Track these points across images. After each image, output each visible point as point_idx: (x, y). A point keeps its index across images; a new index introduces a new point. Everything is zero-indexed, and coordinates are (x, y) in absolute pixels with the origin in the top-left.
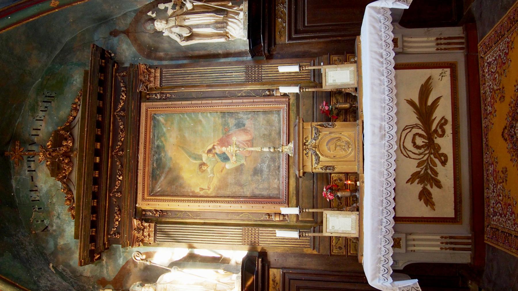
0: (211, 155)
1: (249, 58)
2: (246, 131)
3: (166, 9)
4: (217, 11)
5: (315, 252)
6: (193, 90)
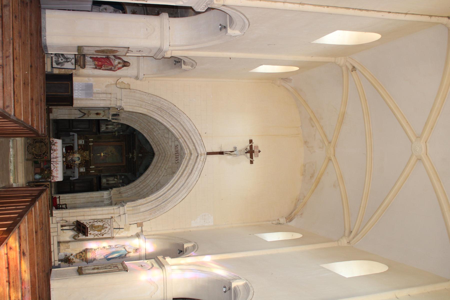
1: (102, 175)
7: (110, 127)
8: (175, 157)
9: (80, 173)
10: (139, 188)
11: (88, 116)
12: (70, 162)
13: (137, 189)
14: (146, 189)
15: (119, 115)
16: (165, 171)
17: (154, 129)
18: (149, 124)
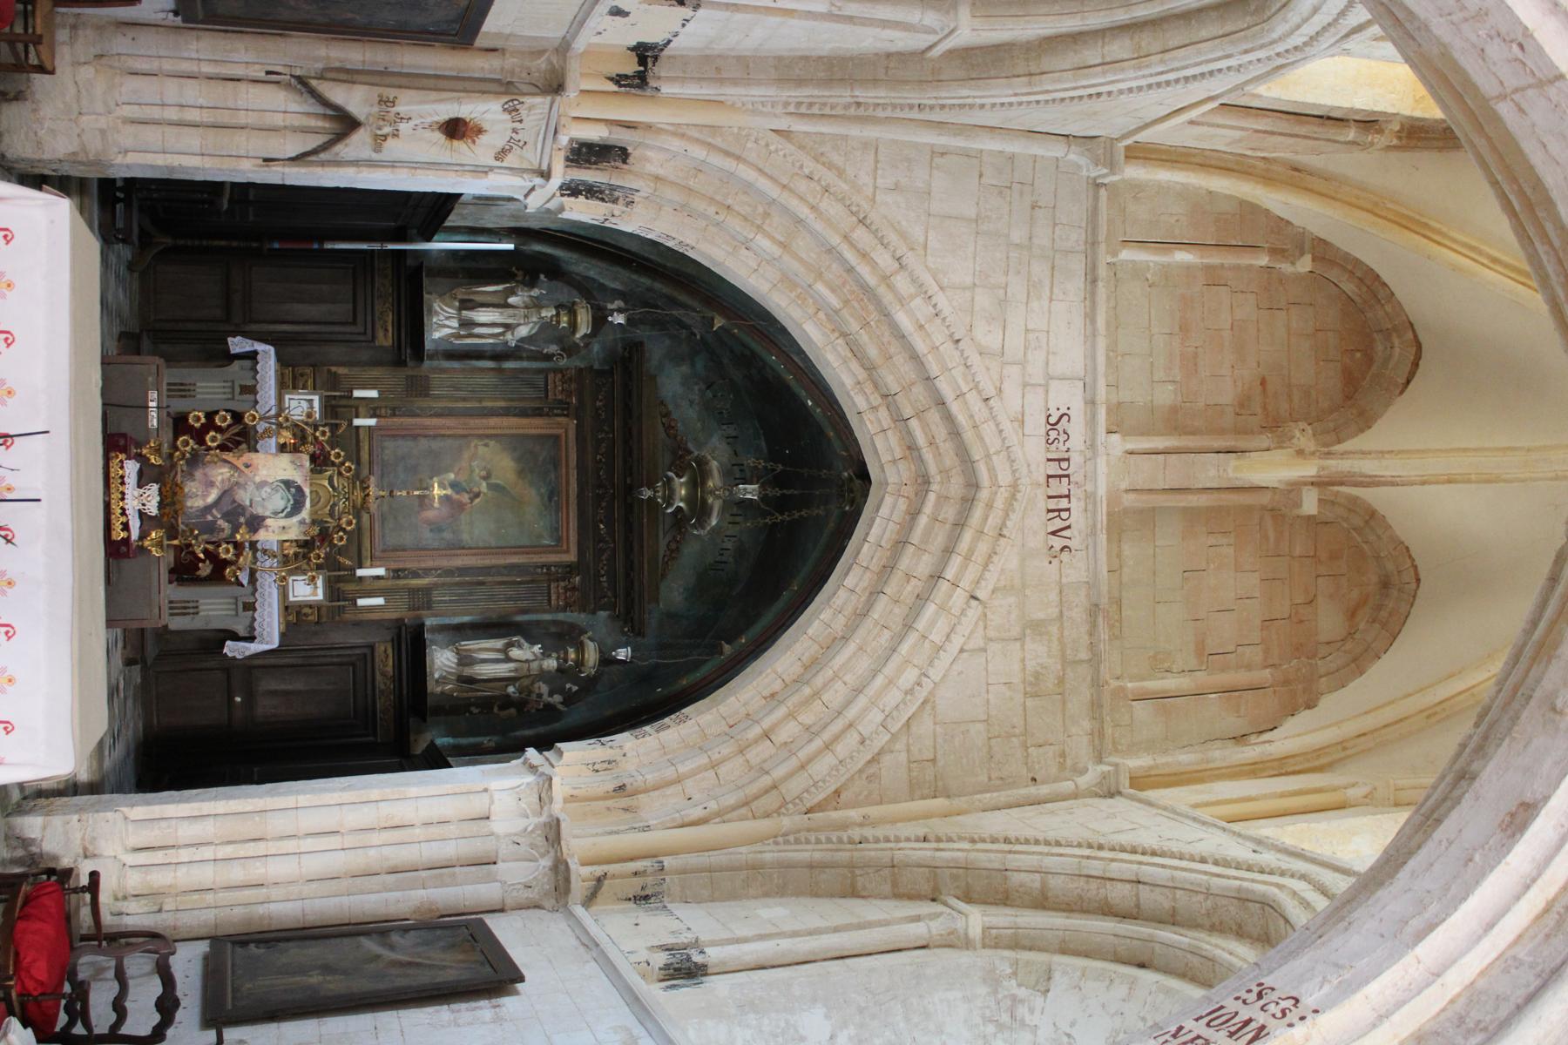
0: (476, 490)
1: (429, 622)
2: (429, 522)
3: (551, 694)
4: (471, 680)
5: (334, 369)
6: (505, 579)
7: (483, 316)
8: (1042, 504)
9: (294, 615)
10: (765, 749)
11: (379, 140)
12: (211, 528)
13: (757, 754)
14: (828, 760)
15: (624, 154)
16: (975, 610)
17: (902, 283)
18: (860, 234)
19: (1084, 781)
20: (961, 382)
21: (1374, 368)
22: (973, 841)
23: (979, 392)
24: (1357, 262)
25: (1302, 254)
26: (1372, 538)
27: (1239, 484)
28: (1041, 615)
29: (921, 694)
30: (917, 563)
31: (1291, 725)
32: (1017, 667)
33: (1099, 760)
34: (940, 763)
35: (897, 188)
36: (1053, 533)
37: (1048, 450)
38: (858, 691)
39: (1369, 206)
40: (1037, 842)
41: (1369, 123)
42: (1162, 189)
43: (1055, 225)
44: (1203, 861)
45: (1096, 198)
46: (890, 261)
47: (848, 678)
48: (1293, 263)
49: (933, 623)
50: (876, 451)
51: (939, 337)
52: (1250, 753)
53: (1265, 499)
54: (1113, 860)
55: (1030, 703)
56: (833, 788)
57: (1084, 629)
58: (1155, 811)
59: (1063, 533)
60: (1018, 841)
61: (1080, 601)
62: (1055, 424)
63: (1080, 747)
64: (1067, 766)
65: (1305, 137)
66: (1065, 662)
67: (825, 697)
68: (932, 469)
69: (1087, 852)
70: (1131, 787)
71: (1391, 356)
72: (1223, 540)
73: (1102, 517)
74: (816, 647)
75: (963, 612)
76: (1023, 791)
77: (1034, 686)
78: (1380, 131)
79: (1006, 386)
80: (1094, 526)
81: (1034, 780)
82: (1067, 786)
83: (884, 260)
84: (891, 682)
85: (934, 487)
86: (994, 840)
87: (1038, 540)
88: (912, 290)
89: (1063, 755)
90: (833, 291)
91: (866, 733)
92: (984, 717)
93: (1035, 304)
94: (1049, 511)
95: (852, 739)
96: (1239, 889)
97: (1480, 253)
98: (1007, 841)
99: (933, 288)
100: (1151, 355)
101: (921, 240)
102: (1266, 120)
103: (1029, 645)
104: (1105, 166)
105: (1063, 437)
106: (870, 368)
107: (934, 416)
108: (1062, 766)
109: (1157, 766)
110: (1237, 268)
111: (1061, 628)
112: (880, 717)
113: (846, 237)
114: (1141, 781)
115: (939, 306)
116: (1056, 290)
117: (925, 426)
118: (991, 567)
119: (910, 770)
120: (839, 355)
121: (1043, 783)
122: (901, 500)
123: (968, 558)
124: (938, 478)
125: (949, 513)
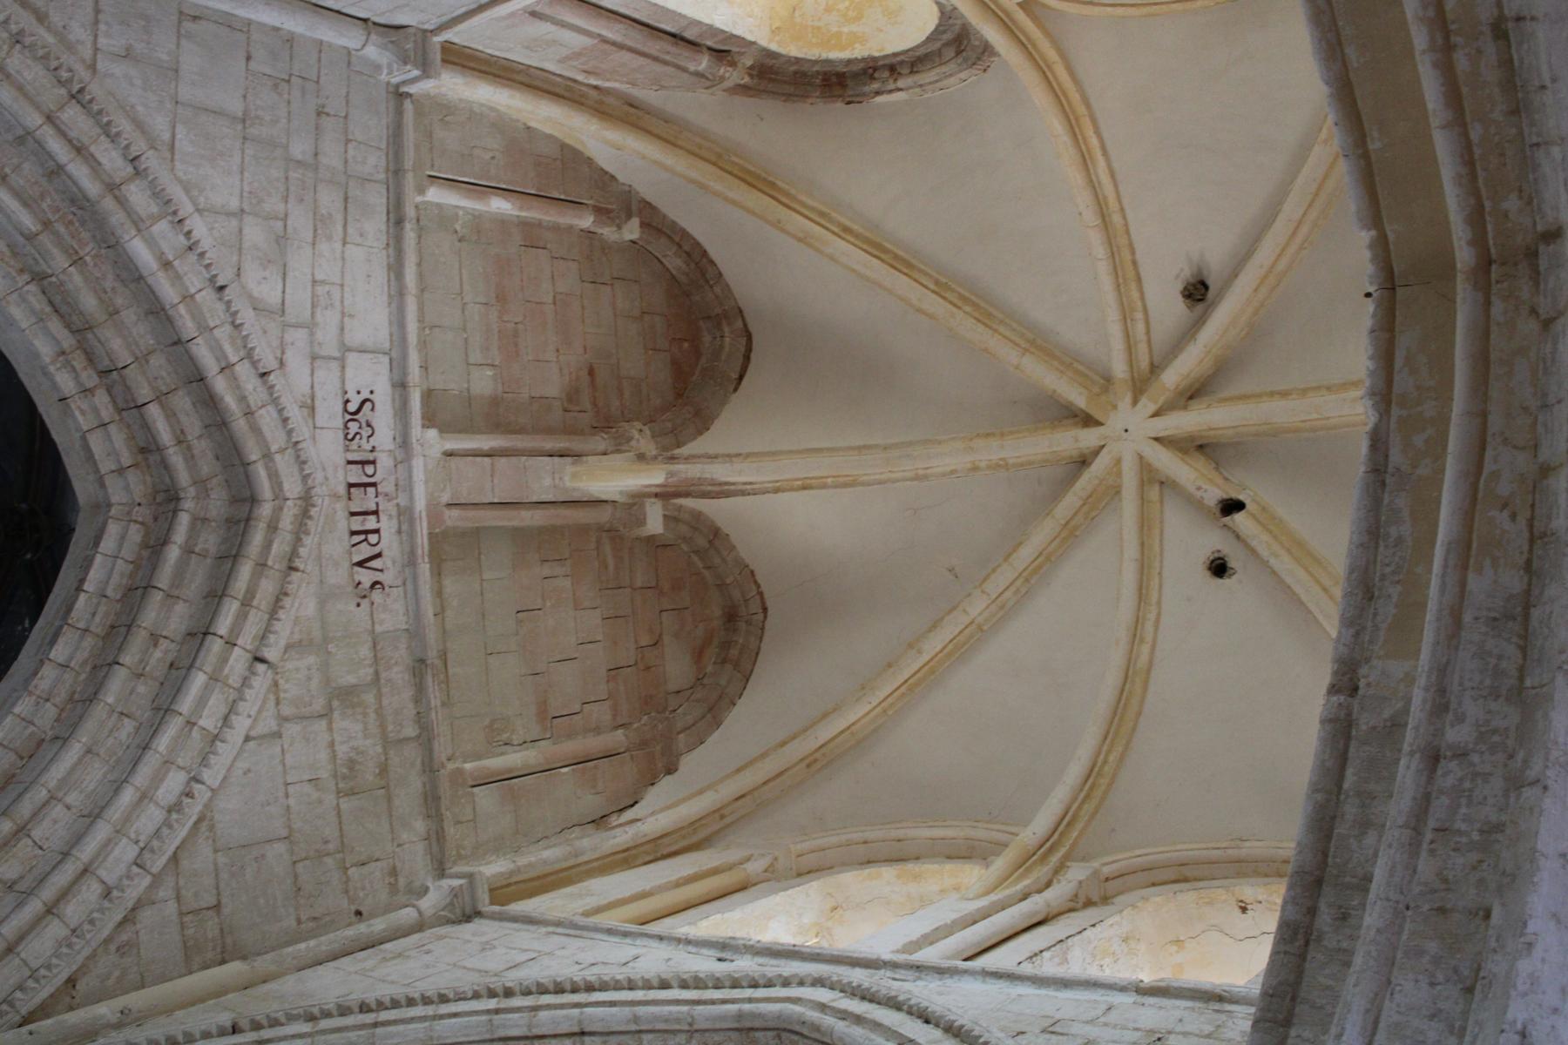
8: (343, 524)
14: (54, 930)
17: (137, 195)
18: (72, 115)
19: (428, 903)
20: (228, 348)
21: (703, 360)
22: (311, 1018)
23: (254, 364)
24: (685, 234)
25: (629, 216)
26: (717, 561)
27: (576, 496)
28: (351, 679)
29: (194, 809)
30: (165, 617)
31: (653, 797)
32: (323, 755)
33: (441, 873)
34: (226, 911)
35: (128, 55)
36: (360, 564)
37: (347, 450)
38: (93, 815)
39: (713, 158)
40: (411, 1002)
41: (723, 50)
42: (474, 116)
43: (348, 141)
44: (664, 985)
45: (399, 112)
46: (120, 162)
47: (73, 798)
48: (619, 227)
49: (202, 702)
50: (90, 456)
51: (194, 282)
52: (620, 837)
53: (603, 516)
54: (376, 1025)
55: (345, 804)
56: (64, 976)
57: (408, 694)
58: (544, 930)
59: (374, 564)
60: (381, 1006)
61: (400, 653)
62: (355, 413)
63: (415, 857)
64: (403, 890)
65: (656, 59)
66: (386, 742)
67: (37, 833)
68: (183, 478)
69: (492, 1004)
70: (492, 903)
71: (722, 347)
72: (558, 570)
73: (423, 540)
74: (12, 757)
75: (245, 682)
76: (350, 932)
77: (347, 778)
78: (733, 64)
79: (289, 356)
80: (412, 553)
81: (359, 913)
82: (407, 915)
83: (111, 159)
84: (144, 797)
85: (188, 504)
86: (344, 1011)
87: (338, 576)
88: (154, 209)
89: (394, 872)
90: (25, 204)
91: (110, 879)
92: (284, 833)
93: (323, 246)
94: (353, 533)
95: (90, 892)
96: (740, 1016)
97: (831, 220)
98: (364, 1008)
99: (186, 208)
100: (464, 330)
101: (166, 136)
102: (618, 26)
103: (340, 723)
104: (416, 67)
105: (366, 432)
106: (82, 330)
107: (182, 402)
108: (393, 889)
109: (519, 870)
110: (556, 228)
111: (379, 696)
112: (131, 852)
113: (50, 119)
114: (505, 892)
115: (196, 235)
116: (350, 230)
117: (171, 415)
118: (281, 614)
119: (183, 926)
120: (33, 311)
121: (373, 916)
122: (134, 527)
123: (246, 603)
124: (192, 492)
125: (210, 541)
